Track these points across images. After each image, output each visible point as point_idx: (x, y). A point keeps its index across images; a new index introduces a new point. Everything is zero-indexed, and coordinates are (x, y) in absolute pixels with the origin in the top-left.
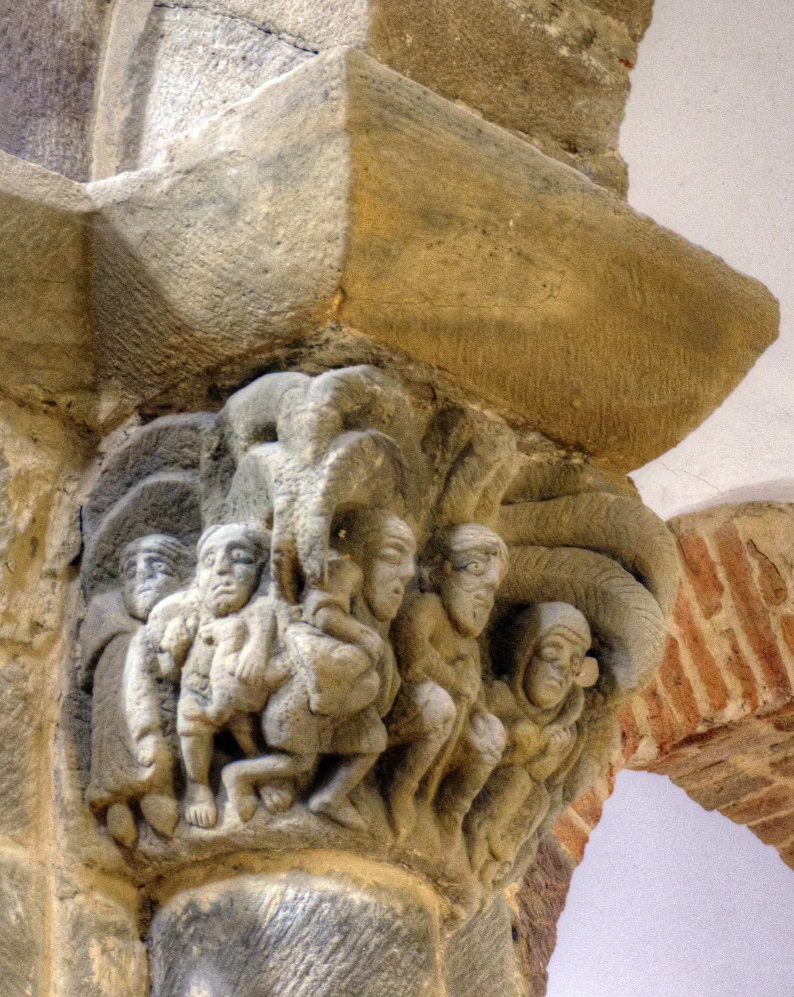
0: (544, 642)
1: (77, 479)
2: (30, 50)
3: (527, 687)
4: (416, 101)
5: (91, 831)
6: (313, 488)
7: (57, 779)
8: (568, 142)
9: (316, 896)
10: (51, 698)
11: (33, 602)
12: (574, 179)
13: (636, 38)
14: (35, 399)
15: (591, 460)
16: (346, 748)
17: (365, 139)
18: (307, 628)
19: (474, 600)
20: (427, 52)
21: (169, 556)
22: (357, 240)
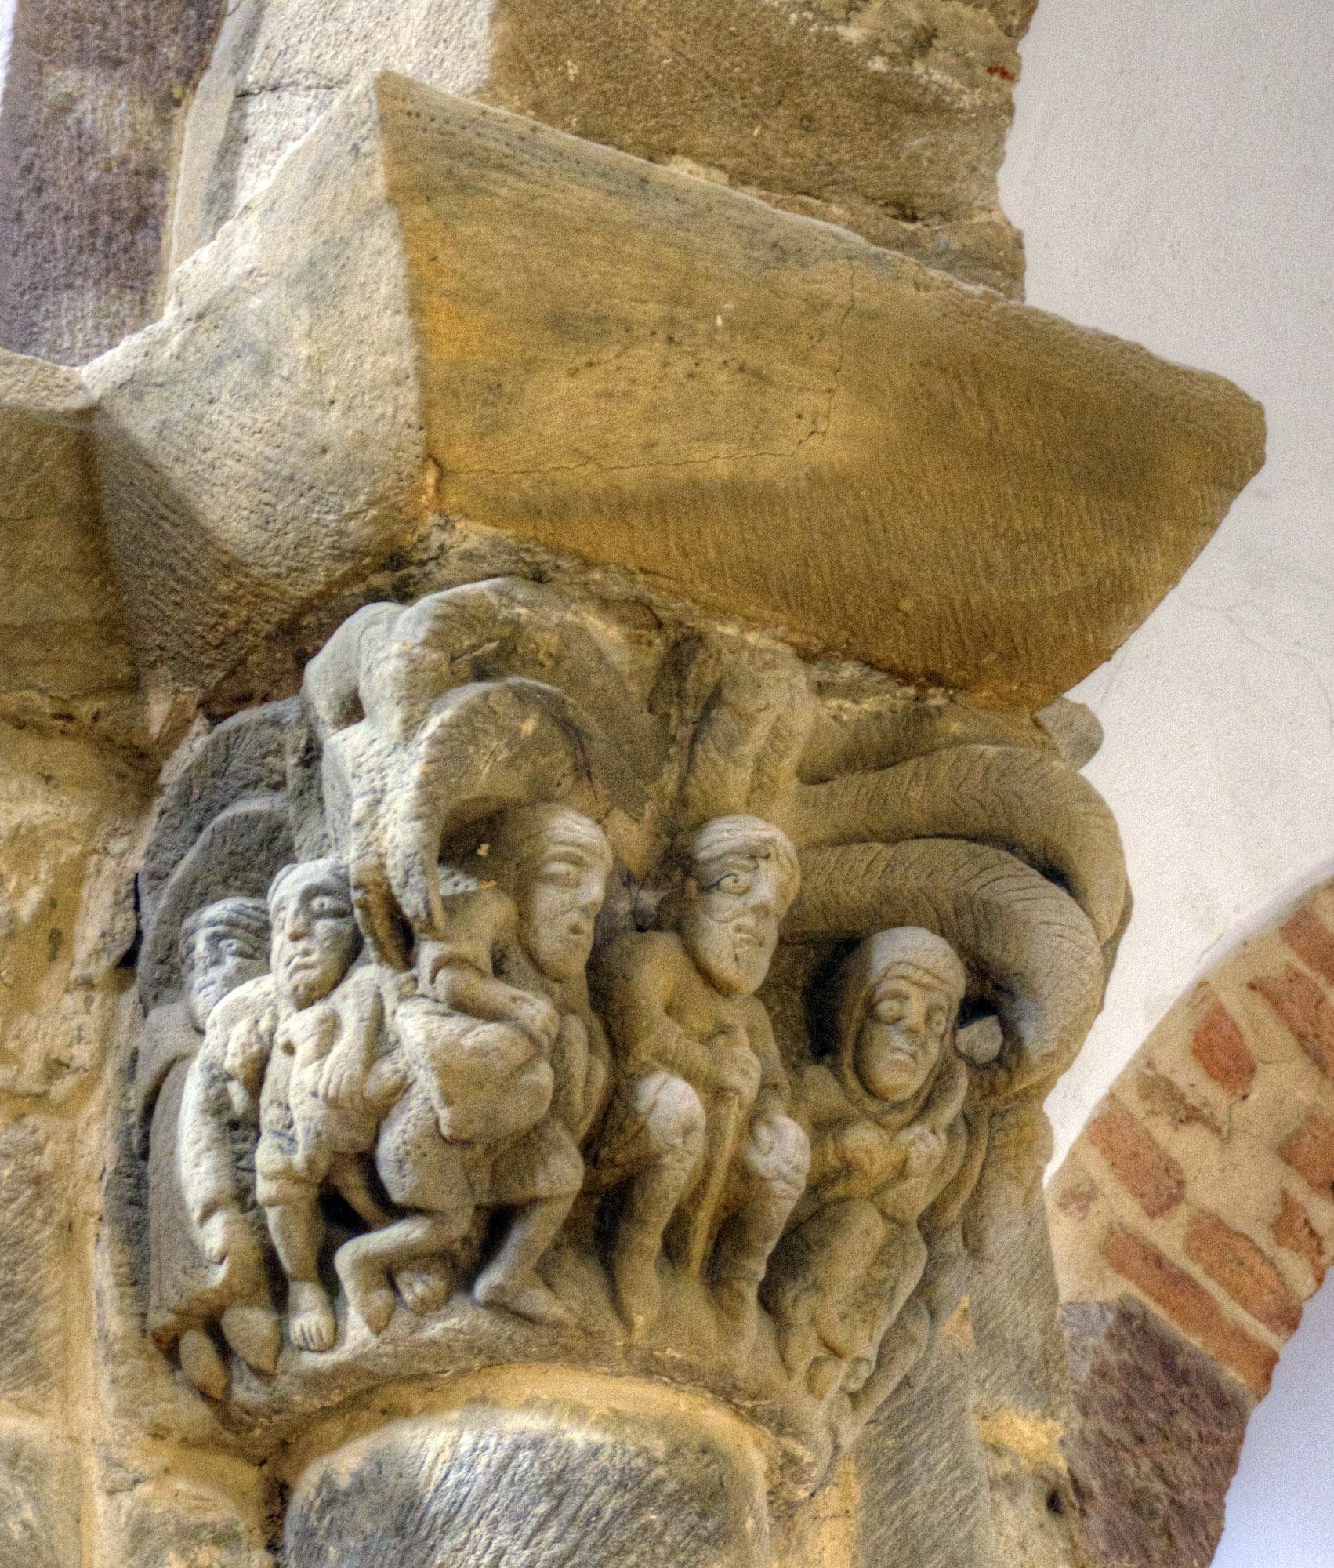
0: (878, 995)
1: (129, 832)
2: (39, 190)
3: (860, 1070)
4: (516, 143)
5: (161, 1380)
6: (404, 778)
7: (100, 1304)
8: (898, 205)
9: (507, 1441)
10: (87, 1177)
11: (50, 1031)
12: (834, 242)
13: (1015, 32)
14: (43, 714)
15: (958, 697)
16: (516, 1193)
17: (425, 210)
18: (427, 1005)
19: (738, 934)
20: (609, 86)
21: (247, 928)
22: (437, 375)
